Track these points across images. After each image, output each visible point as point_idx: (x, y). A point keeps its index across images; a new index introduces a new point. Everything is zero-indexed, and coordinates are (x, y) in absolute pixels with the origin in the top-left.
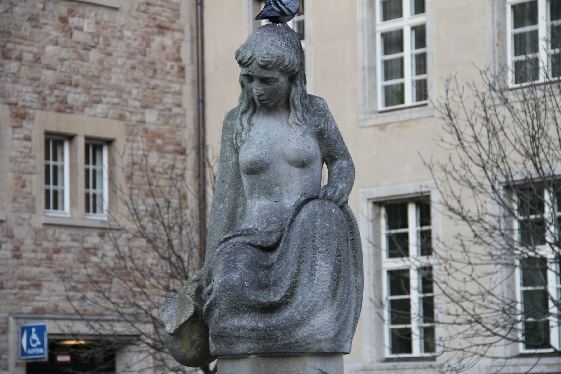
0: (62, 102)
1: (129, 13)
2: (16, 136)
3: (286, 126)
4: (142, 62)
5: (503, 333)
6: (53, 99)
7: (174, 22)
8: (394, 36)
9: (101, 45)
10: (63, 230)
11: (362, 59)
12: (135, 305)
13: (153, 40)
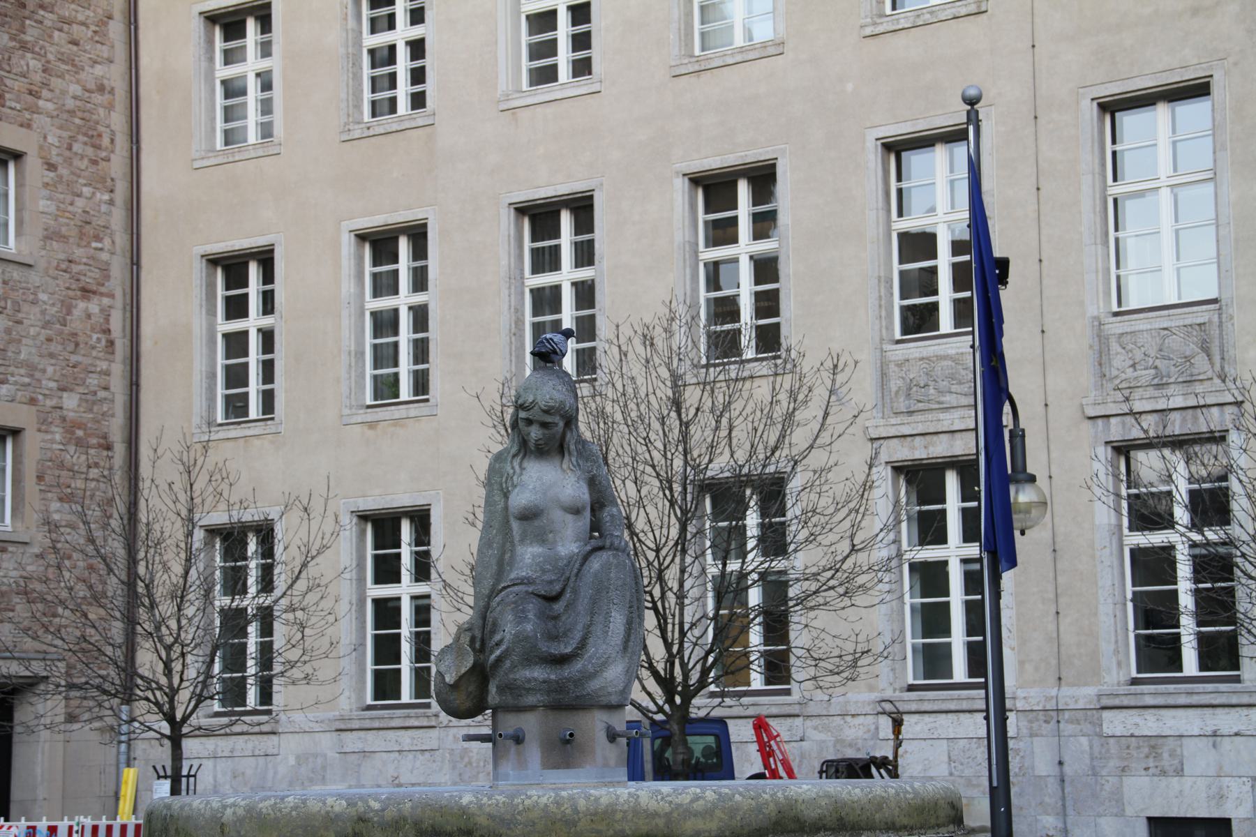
1: (46, 270)
3: (559, 471)
4: (60, 333)
7: (103, 285)
9: (9, 311)
11: (349, 343)
13: (76, 307)
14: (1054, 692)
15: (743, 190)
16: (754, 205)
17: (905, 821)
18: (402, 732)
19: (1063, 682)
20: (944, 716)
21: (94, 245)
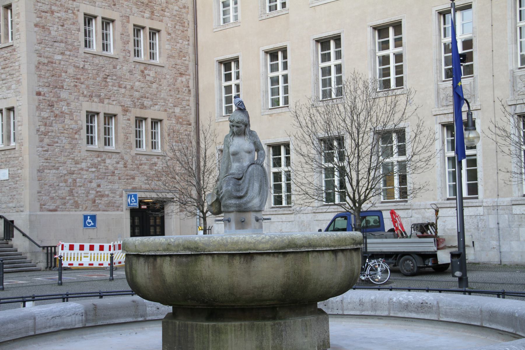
0: (142, 105)
2: (124, 119)
5: (316, 198)
6: (139, 104)
8: (275, 78)
10: (143, 156)
11: (263, 88)
12: (175, 187)
14: (496, 200)
15: (391, 30)
16: (395, 36)
17: (333, 244)
18: (283, 216)
19: (499, 196)
20: (475, 208)
21: (183, 59)
